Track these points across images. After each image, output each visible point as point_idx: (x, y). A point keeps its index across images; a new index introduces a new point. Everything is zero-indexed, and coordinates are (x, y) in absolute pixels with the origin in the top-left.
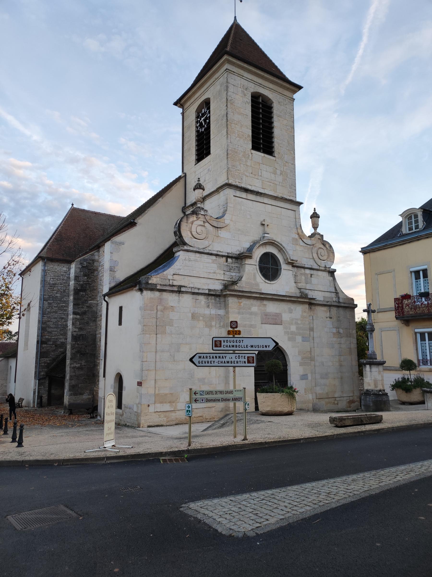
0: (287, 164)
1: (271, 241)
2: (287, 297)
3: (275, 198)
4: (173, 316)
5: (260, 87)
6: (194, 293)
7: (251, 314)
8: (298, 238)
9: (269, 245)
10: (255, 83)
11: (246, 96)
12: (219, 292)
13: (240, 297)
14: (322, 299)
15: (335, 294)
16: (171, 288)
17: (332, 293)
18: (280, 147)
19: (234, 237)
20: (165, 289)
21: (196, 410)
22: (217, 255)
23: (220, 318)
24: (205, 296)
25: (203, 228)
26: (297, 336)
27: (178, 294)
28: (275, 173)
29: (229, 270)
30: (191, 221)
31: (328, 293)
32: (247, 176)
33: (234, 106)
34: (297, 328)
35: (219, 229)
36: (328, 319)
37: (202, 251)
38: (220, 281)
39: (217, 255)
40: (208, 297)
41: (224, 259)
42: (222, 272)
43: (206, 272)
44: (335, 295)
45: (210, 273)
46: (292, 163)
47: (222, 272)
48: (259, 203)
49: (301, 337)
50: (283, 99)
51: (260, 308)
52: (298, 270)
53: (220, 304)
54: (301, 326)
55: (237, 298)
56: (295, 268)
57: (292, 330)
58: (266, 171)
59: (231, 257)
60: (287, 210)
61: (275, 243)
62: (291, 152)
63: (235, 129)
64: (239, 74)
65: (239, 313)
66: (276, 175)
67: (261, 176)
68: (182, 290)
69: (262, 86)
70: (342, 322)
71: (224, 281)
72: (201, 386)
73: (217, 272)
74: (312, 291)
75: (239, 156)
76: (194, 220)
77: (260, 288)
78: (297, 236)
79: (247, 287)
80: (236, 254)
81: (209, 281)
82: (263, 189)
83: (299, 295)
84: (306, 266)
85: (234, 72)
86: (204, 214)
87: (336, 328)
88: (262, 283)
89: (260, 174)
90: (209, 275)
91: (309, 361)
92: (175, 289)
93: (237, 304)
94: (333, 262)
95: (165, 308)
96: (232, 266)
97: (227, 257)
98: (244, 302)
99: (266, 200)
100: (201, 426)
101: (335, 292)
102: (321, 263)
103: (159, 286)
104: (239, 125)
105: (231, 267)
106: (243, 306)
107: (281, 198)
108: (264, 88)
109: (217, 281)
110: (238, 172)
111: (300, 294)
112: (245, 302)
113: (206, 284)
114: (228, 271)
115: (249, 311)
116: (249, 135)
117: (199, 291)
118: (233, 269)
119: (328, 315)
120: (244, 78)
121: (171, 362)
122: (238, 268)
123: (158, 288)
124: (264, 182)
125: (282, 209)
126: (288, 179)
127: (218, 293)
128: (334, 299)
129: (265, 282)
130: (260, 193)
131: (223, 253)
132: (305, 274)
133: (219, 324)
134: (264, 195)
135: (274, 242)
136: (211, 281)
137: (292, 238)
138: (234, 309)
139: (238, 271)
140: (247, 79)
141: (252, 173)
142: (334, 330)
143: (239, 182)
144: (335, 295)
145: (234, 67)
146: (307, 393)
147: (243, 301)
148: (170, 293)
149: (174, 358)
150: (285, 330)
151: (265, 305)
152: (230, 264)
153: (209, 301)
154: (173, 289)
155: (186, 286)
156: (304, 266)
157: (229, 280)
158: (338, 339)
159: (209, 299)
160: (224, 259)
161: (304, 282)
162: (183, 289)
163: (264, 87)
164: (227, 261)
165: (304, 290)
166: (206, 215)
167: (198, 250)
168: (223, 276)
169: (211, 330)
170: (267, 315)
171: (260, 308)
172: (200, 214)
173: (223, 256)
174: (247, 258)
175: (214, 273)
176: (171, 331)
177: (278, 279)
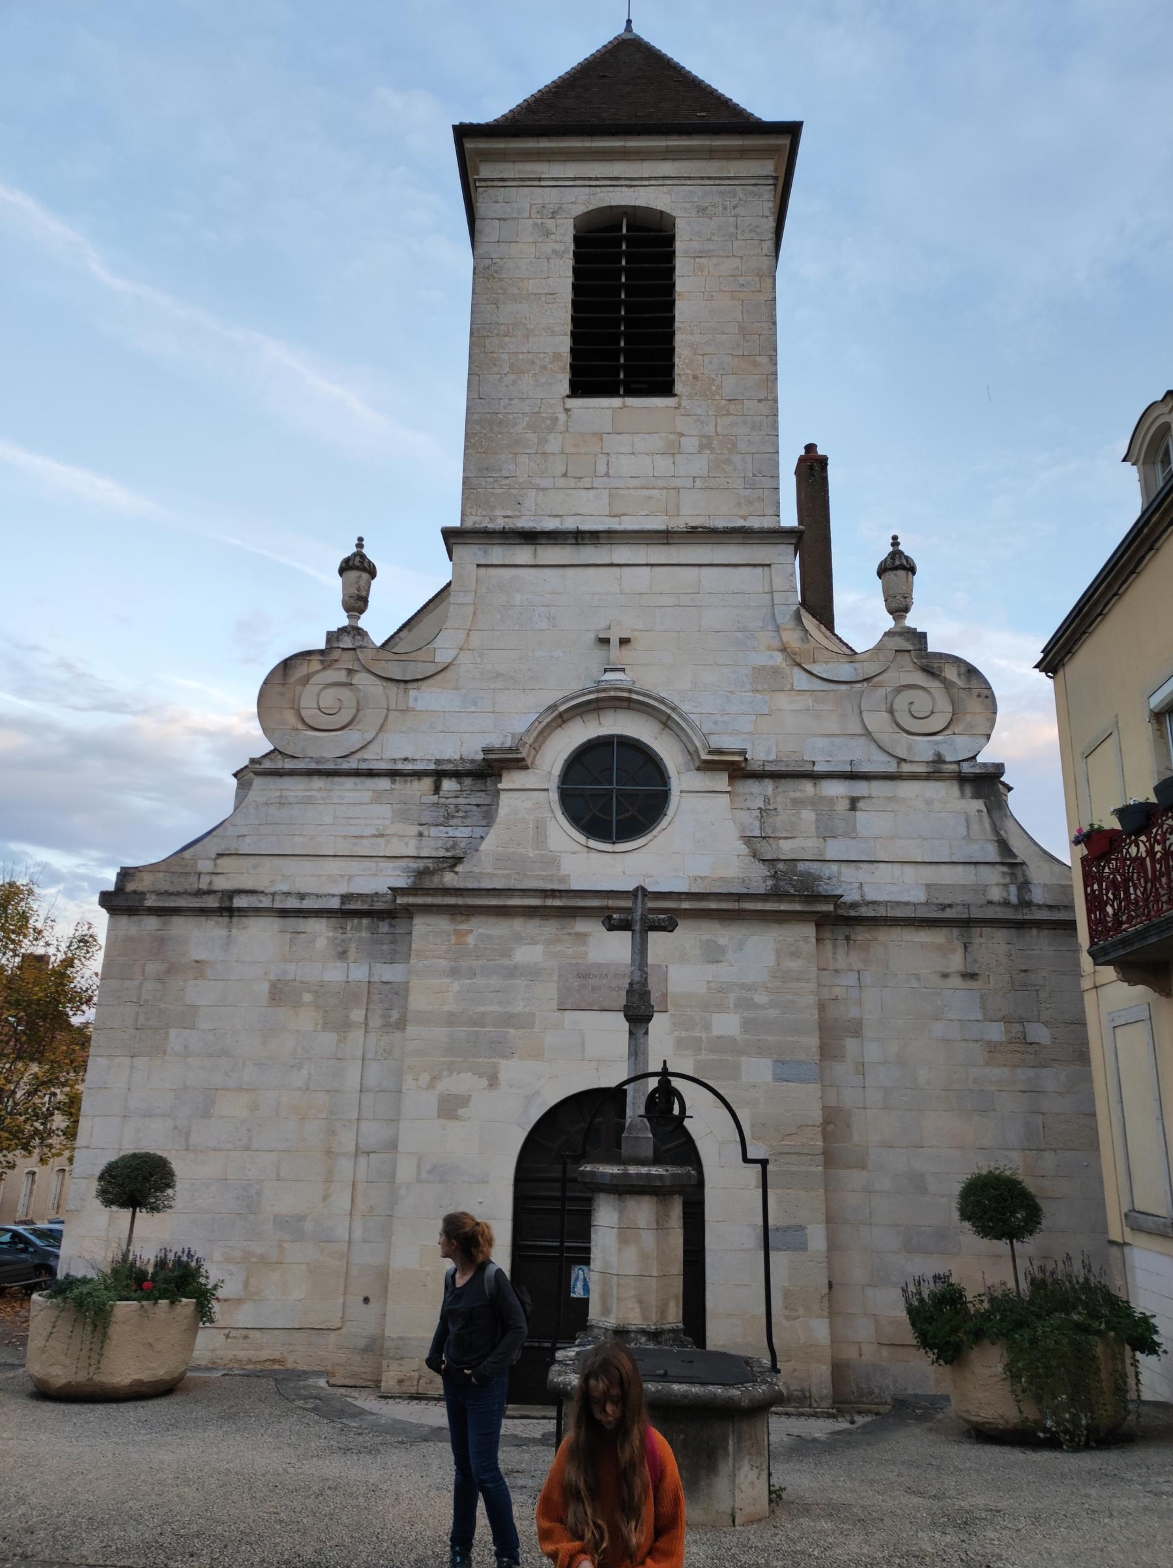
0: (732, 408)
1: (613, 694)
2: (680, 900)
3: (665, 537)
4: (198, 993)
5: (619, 188)
6: (284, 913)
7: (512, 972)
8: (784, 665)
9: (615, 708)
10: (593, 183)
11: (553, 237)
12: (383, 899)
13: (462, 914)
14: (919, 896)
15: (1005, 869)
16: (197, 900)
17: (985, 871)
18: (703, 355)
19: (475, 704)
20: (172, 904)
21: (257, 1334)
22: (393, 774)
23: (390, 996)
24: (333, 920)
25: (345, 694)
26: (743, 1059)
27: (226, 919)
28: (673, 451)
29: (442, 819)
30: (303, 674)
31: (960, 868)
32: (544, 489)
33: (501, 279)
34: (746, 1025)
35: (410, 686)
36: (956, 981)
37: (330, 766)
38: (402, 863)
39: (393, 774)
40: (344, 920)
41: (427, 783)
42: (414, 830)
43: (345, 837)
44: (1004, 873)
45: (362, 837)
46: (762, 397)
47: (414, 830)
48: (592, 570)
49: (769, 1062)
50: (722, 193)
51: (558, 948)
52: (780, 790)
53: (393, 942)
54: (773, 1013)
55: (447, 917)
56: (766, 780)
57: (720, 1033)
58: (633, 453)
59: (456, 775)
60: (731, 569)
61: (634, 696)
62: (758, 358)
63: (501, 351)
64: (522, 179)
65: (454, 973)
66: (678, 457)
67: (607, 475)
68: (234, 906)
69: (624, 183)
70: (1043, 995)
71: (419, 860)
72: (286, 1245)
73: (389, 831)
74: (861, 865)
75: (512, 430)
76: (311, 670)
77: (563, 872)
78: (779, 659)
79: (501, 872)
80: (473, 761)
81: (355, 866)
82: (614, 516)
83: (760, 887)
84: (818, 768)
85: (502, 180)
86: (350, 646)
87: (1007, 1020)
88: (574, 853)
89: (602, 469)
90: (355, 844)
91: (813, 1169)
92: (212, 902)
93: (449, 941)
94: (988, 736)
95: (172, 969)
96: (456, 806)
97: (439, 775)
98: (481, 931)
99: (622, 554)
100: (786, 1414)
101: (998, 860)
102: (910, 748)
103: (154, 897)
104: (519, 333)
105: (452, 809)
106: (476, 945)
107: (688, 532)
108: (631, 186)
109: (390, 865)
110: (506, 485)
111: (770, 883)
112: (480, 930)
113: (342, 876)
114: (437, 825)
115: (505, 962)
116: (557, 356)
117: (304, 902)
118: (461, 814)
119: (956, 961)
120: (542, 183)
121: (174, 1152)
122: (484, 808)
123: (148, 903)
124: (621, 492)
125: (704, 570)
126: (736, 458)
127: (379, 906)
128: (996, 894)
129: (586, 849)
130: (588, 535)
131: (419, 762)
132: (815, 802)
133: (384, 1016)
134: (610, 538)
135: (626, 694)
136: (367, 863)
137: (753, 668)
138: (435, 957)
139: (484, 818)
140: (558, 183)
141: (565, 475)
142: (996, 1032)
143: (505, 517)
144: (1004, 873)
145: (510, 166)
146: (801, 1311)
147: (479, 927)
148: (197, 918)
149: (187, 1139)
150: (683, 1034)
151: (582, 937)
152: (447, 798)
153: (349, 935)
154: (203, 905)
155: (261, 889)
156: (808, 767)
157: (442, 853)
158: (1019, 1071)
159: (348, 928)
160: (427, 783)
161: (812, 830)
162: (239, 902)
163: (631, 182)
164: (437, 789)
165: (815, 865)
166: (360, 647)
167: (313, 766)
168: (413, 843)
169: (345, 1038)
170: (587, 976)
171: (558, 948)
172: (339, 648)
173: (418, 775)
174: (509, 769)
175: (376, 836)
176: (186, 1047)
177: (655, 832)
